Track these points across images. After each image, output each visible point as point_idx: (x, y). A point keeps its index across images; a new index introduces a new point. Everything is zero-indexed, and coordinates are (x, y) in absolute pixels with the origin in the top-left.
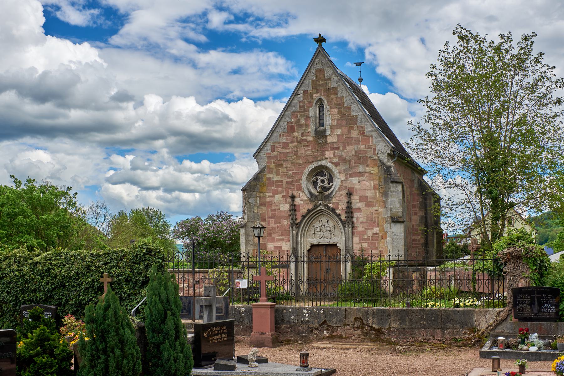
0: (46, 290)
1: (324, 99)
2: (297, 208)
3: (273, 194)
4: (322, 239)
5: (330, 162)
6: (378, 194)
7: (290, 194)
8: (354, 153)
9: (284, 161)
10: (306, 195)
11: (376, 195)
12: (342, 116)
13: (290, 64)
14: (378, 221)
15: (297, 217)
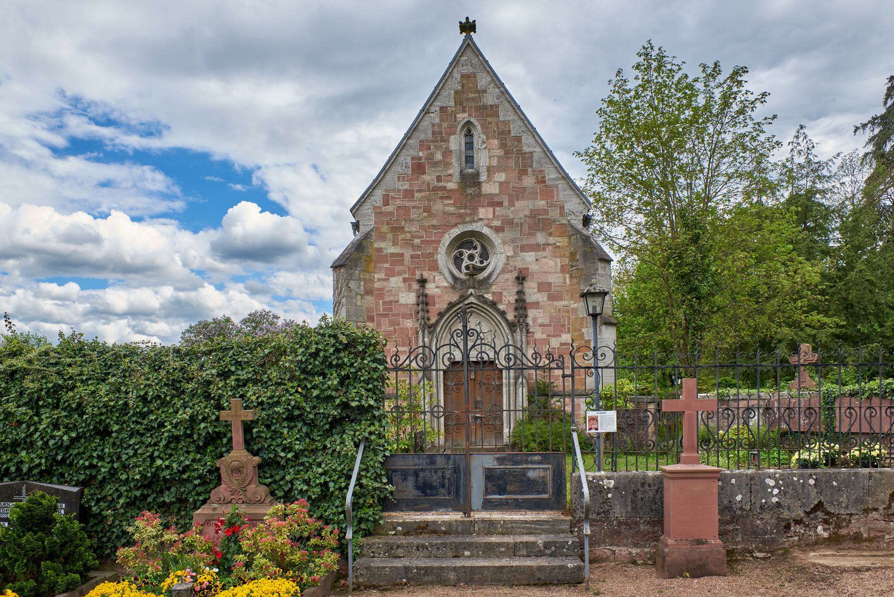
0: (51, 442)
1: (476, 123)
5: (486, 226)
6: (568, 280)
7: (418, 277)
8: (527, 213)
10: (446, 279)
11: (565, 282)
14: (569, 324)
15: (430, 315)
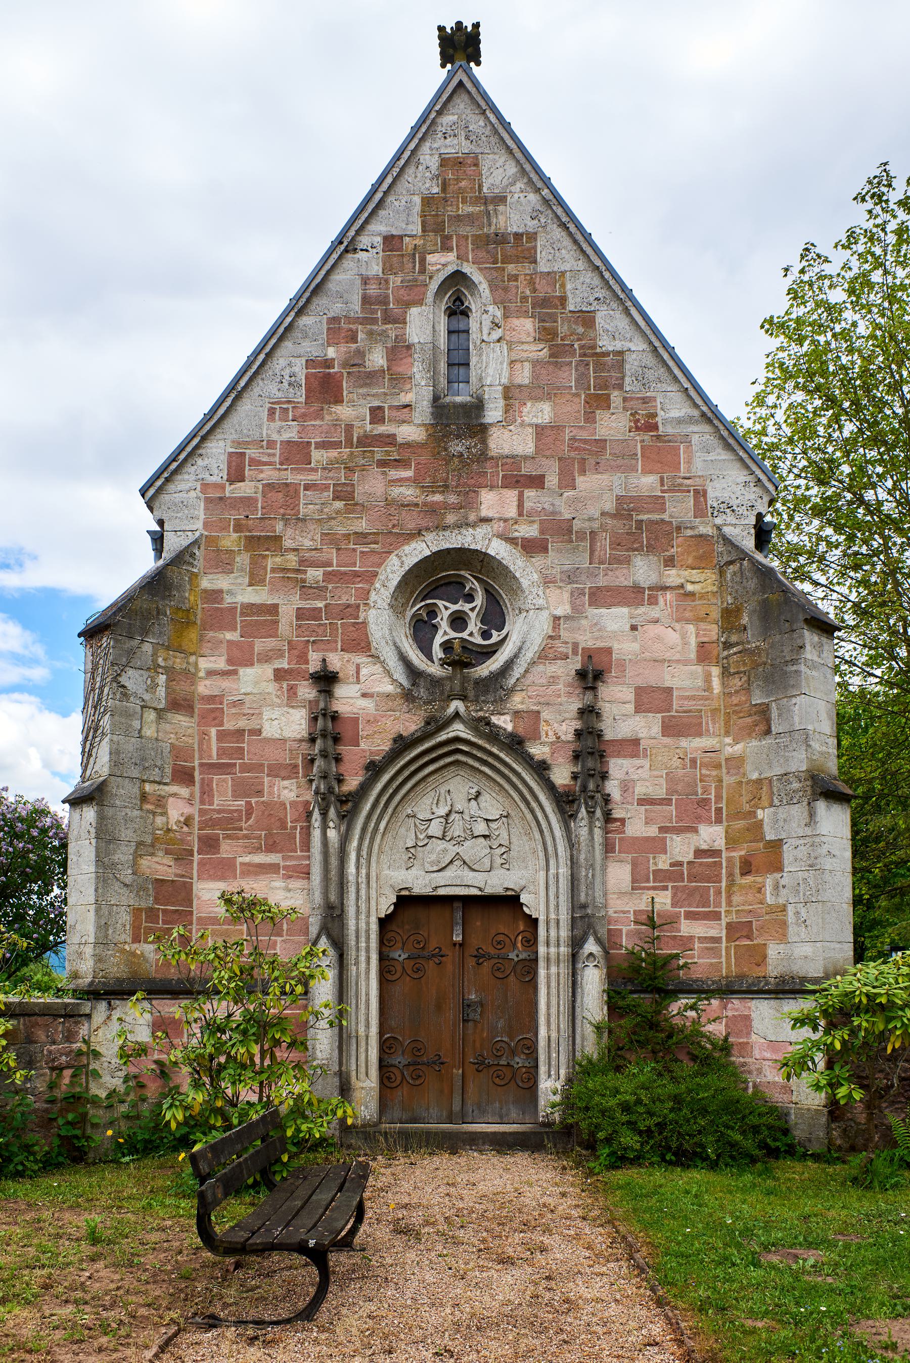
1: (477, 277)
2: (346, 731)
3: (230, 661)
4: (448, 873)
5: (500, 536)
7: (314, 666)
8: (609, 505)
9: (286, 522)
11: (709, 688)
12: (558, 352)
13: (29, 637)
14: (719, 798)
15: (342, 769)
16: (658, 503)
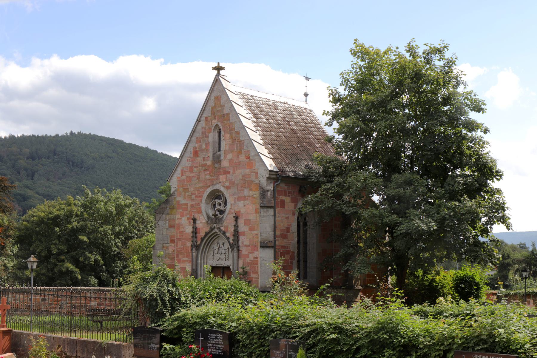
8: (241, 177)
11: (257, 219)
16: (249, 176)
